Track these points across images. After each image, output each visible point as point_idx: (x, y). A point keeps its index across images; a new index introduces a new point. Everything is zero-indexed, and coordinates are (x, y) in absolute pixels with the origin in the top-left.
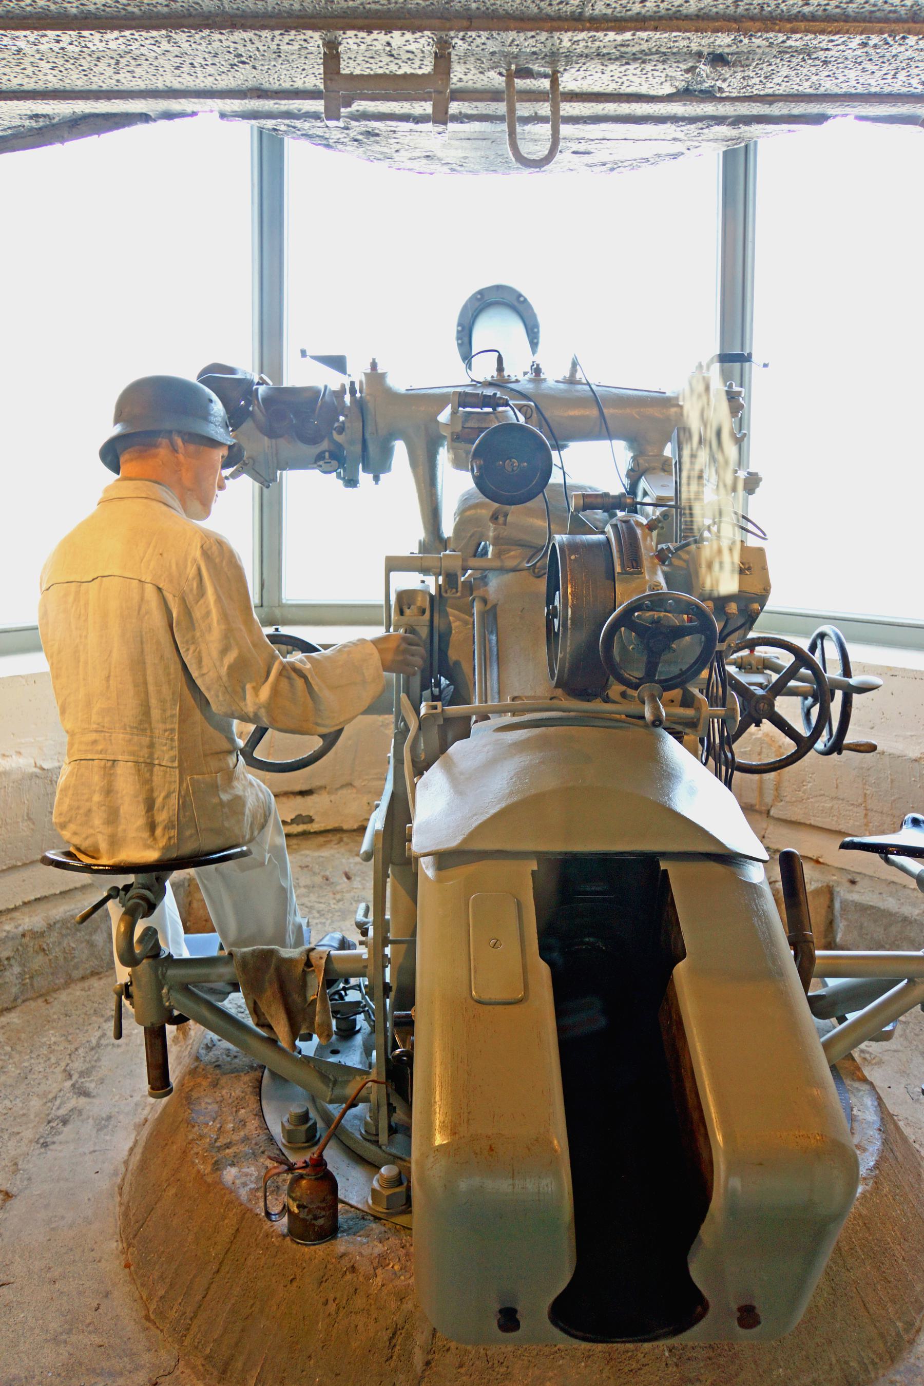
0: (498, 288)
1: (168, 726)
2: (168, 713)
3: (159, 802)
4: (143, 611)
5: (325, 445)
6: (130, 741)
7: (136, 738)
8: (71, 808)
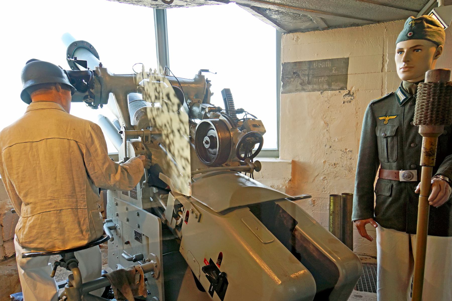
0: (82, 42)
1: (83, 193)
2: (82, 189)
3: (82, 222)
4: (71, 151)
5: (87, 93)
6: (68, 201)
7: (71, 200)
8: (38, 233)
